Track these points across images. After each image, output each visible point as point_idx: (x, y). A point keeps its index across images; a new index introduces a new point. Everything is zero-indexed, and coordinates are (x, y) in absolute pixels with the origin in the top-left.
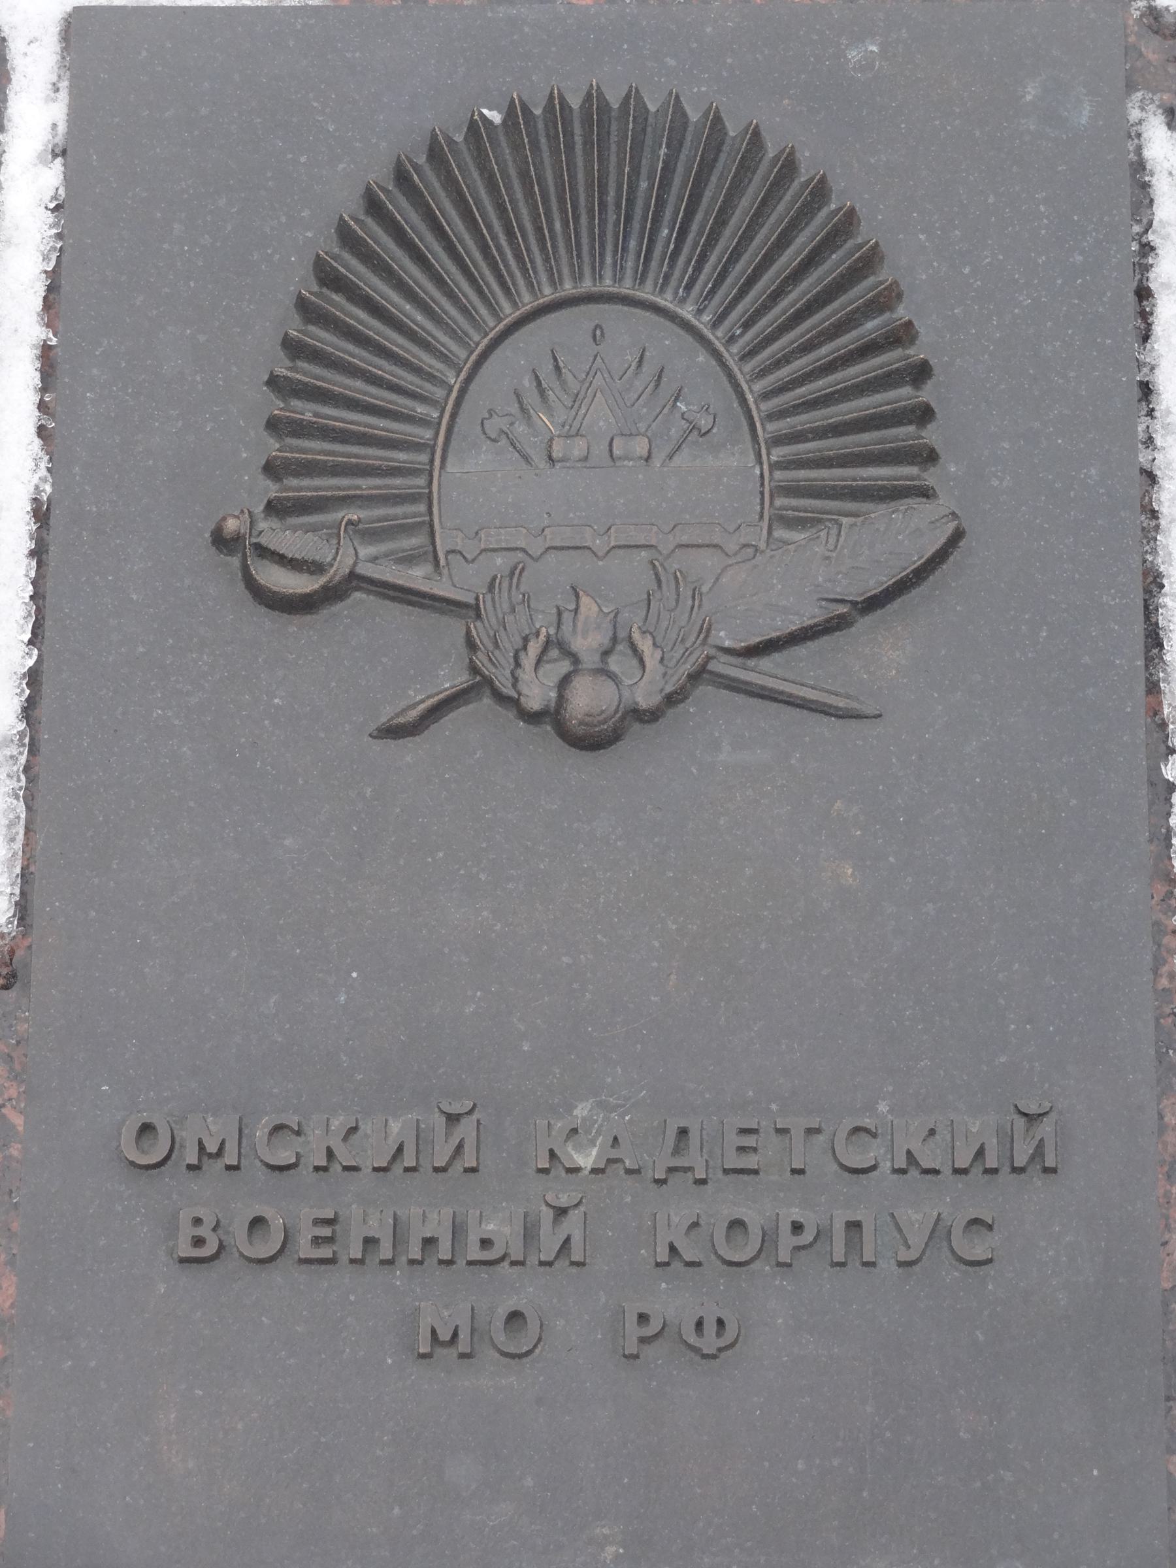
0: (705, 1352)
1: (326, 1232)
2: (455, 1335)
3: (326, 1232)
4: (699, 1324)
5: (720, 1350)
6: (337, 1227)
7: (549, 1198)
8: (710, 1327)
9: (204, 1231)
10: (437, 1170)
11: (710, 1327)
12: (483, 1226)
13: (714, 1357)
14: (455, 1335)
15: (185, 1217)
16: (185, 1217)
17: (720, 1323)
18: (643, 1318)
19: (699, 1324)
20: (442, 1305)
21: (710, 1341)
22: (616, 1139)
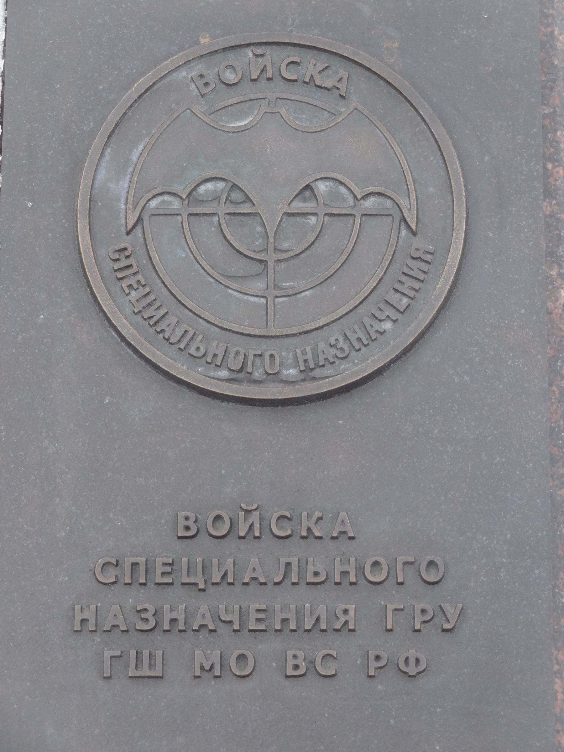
0: (410, 674)
1: (169, 569)
2: (212, 666)
3: (169, 569)
4: (407, 660)
5: (419, 673)
6: (174, 567)
7: (243, 506)
8: (412, 662)
9: (190, 523)
10: (252, 80)
11: (412, 662)
12: (202, 560)
13: (414, 676)
14: (212, 666)
15: (290, 653)
16: (290, 653)
17: (417, 661)
18: (378, 658)
19: (407, 660)
20: (207, 653)
21: (412, 670)
22: (169, 324)
